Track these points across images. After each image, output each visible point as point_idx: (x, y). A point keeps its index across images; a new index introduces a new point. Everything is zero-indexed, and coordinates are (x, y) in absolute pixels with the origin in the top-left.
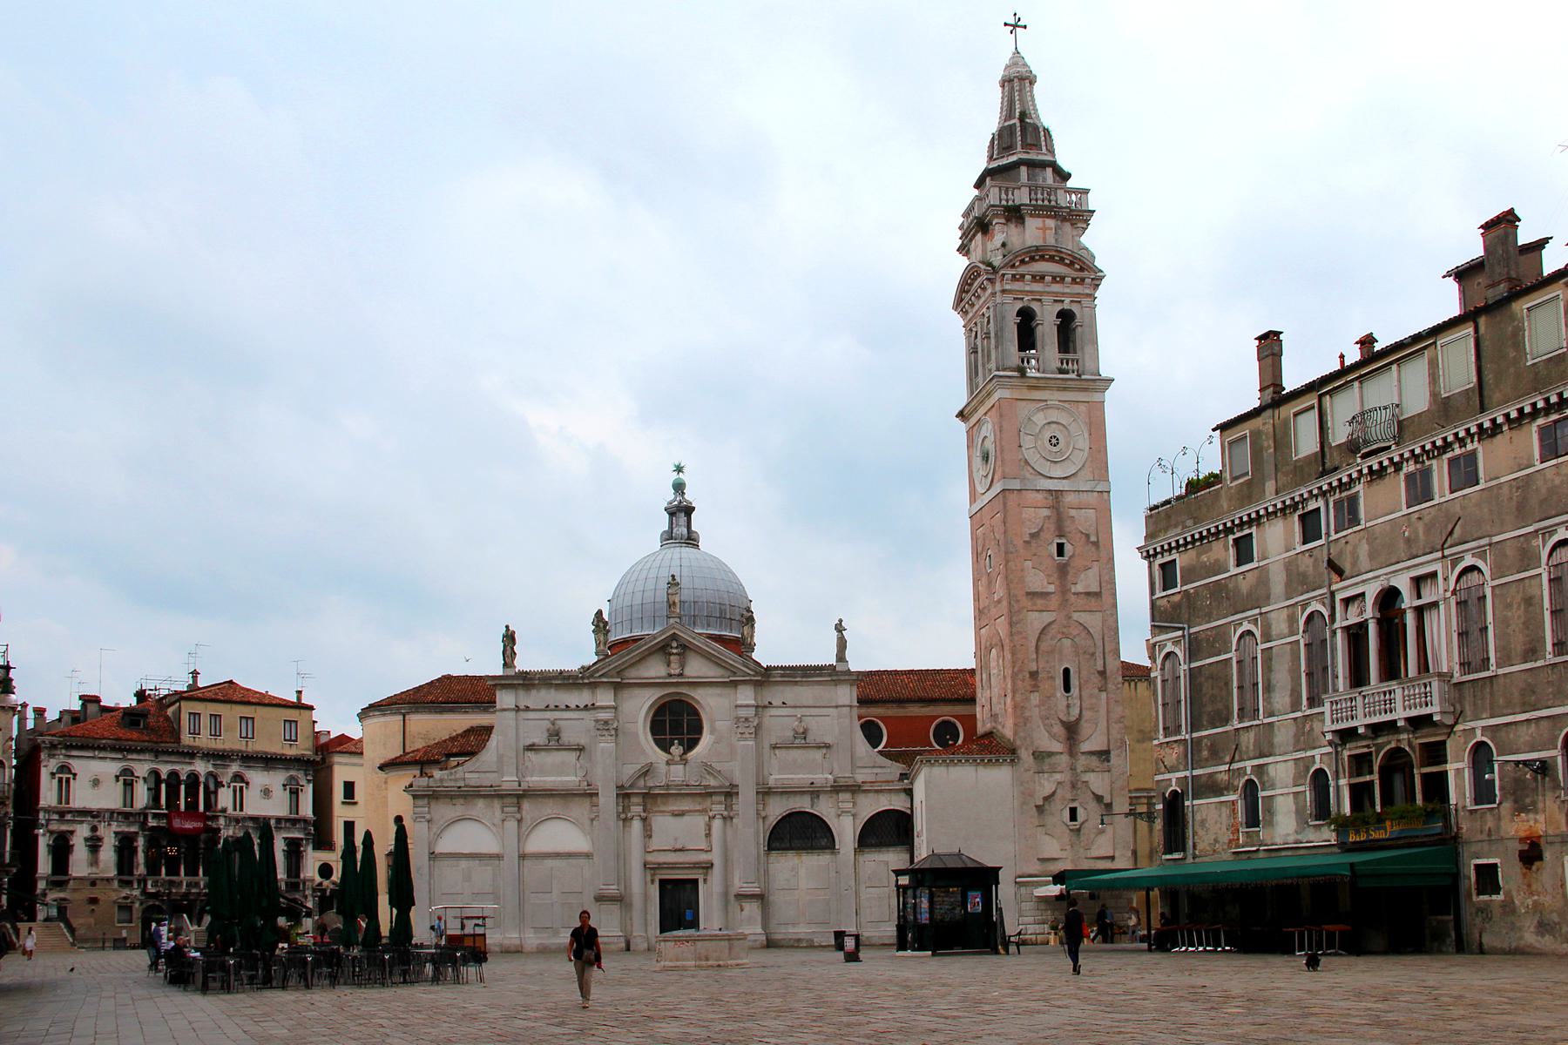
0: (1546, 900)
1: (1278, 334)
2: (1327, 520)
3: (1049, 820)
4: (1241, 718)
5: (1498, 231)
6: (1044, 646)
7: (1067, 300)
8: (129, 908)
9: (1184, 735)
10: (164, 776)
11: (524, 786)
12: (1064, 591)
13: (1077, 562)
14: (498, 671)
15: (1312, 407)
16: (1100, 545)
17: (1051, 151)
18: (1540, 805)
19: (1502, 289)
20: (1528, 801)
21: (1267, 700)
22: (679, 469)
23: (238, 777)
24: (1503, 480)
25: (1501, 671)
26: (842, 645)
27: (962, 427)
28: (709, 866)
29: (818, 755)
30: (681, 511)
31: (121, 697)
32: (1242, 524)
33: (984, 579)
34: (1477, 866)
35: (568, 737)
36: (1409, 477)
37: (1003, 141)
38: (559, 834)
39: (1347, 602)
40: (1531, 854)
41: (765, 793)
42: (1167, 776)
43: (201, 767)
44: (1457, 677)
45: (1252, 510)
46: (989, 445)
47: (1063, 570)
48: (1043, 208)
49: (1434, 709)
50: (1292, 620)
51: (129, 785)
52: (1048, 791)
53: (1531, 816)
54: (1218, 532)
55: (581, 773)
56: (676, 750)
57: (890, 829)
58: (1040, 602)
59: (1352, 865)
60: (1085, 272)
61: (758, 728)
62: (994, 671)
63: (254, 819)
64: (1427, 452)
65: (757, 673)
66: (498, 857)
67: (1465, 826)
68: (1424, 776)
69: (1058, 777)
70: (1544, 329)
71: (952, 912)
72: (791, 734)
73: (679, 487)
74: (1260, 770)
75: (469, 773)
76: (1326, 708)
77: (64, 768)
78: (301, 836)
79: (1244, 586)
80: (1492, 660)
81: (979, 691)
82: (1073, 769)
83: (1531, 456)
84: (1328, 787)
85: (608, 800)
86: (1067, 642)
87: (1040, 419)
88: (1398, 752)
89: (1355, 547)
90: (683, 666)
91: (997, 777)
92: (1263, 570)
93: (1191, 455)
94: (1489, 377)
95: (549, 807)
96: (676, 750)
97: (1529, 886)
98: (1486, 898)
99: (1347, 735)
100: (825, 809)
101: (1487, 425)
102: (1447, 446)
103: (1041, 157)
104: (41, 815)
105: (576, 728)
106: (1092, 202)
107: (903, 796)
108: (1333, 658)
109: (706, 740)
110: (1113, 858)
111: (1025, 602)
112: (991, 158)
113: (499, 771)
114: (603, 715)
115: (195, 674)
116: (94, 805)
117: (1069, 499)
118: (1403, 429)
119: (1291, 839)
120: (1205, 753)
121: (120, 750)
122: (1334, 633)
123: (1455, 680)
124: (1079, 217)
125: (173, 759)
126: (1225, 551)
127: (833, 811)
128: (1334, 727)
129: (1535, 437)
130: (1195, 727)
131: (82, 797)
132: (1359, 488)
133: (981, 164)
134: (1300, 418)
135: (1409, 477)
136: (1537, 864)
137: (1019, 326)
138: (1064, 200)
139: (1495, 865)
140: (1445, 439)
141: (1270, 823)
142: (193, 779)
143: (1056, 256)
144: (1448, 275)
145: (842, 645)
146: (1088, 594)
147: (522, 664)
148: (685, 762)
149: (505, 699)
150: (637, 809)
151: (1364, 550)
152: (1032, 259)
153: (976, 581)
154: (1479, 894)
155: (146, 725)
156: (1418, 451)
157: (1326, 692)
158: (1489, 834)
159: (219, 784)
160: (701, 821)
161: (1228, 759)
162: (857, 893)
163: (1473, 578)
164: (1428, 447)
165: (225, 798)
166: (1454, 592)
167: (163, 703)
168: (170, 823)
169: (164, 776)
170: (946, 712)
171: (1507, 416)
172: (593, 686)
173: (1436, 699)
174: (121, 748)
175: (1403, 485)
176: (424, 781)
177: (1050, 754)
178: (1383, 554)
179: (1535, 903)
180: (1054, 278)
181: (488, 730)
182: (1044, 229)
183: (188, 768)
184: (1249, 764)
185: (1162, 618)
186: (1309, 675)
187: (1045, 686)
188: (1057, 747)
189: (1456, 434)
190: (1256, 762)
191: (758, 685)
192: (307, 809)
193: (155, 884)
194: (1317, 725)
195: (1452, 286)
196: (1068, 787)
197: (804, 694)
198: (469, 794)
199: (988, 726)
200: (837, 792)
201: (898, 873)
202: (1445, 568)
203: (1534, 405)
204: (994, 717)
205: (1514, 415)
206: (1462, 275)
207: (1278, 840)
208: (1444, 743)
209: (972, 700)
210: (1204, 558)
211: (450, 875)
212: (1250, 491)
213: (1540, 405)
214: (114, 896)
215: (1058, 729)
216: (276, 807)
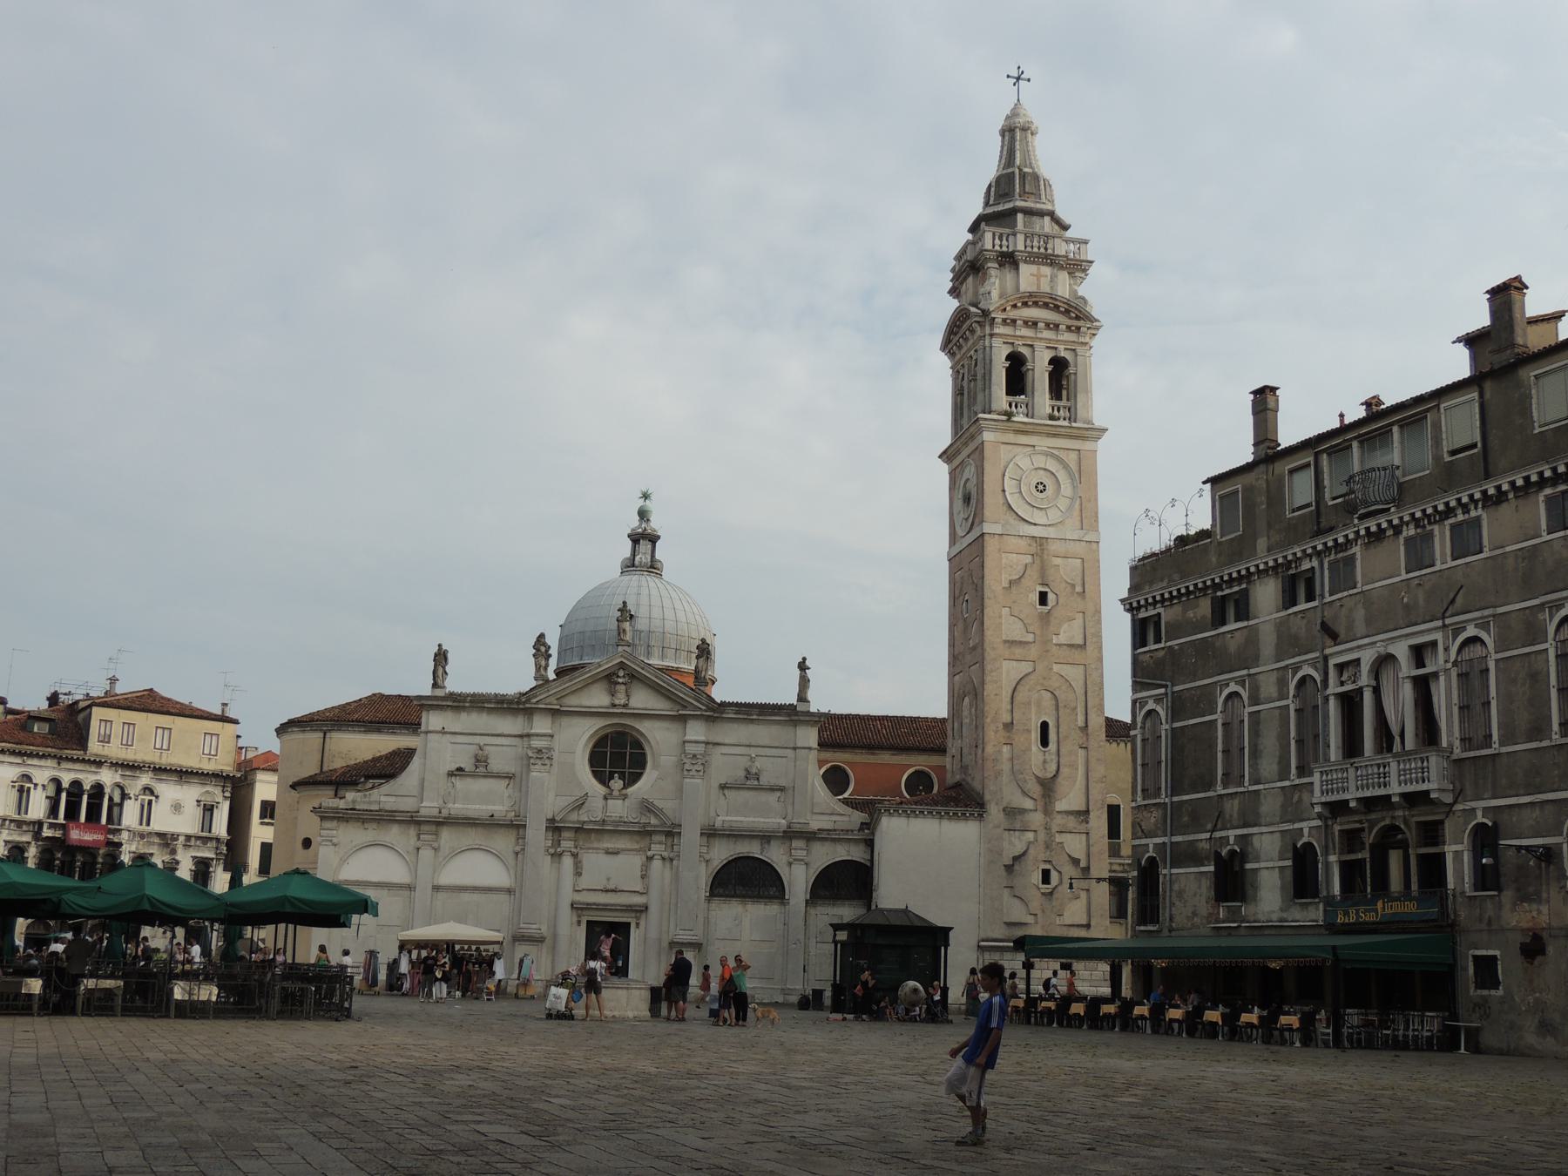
1: (1273, 389)
2: (1324, 580)
4: (1225, 785)
6: (1019, 697)
9: (1163, 798)
10: (65, 785)
11: (445, 813)
14: (426, 690)
15: (1307, 465)
18: (1544, 895)
20: (1531, 889)
22: (646, 496)
23: (148, 790)
24: (1508, 549)
25: (1504, 750)
26: (804, 682)
29: (772, 798)
30: (643, 538)
32: (1231, 580)
33: (960, 625)
34: (1475, 957)
35: (496, 765)
36: (1408, 540)
37: (1002, 187)
38: (479, 866)
39: (1341, 667)
40: (1533, 948)
42: (1144, 841)
43: (107, 777)
44: (1458, 752)
45: (1242, 568)
46: (972, 486)
47: (1045, 619)
48: (1038, 256)
50: (1282, 684)
51: (23, 793)
52: (1018, 850)
53: (1534, 906)
54: (1206, 588)
56: (617, 784)
57: (849, 881)
58: (1018, 651)
59: (1334, 948)
62: (966, 721)
63: (161, 835)
64: (1429, 516)
65: (709, 709)
67: (1463, 914)
68: (1421, 857)
70: (1553, 400)
71: (884, 964)
72: (742, 774)
73: (643, 514)
75: (383, 796)
78: (211, 855)
79: (1233, 645)
80: (1495, 737)
81: (950, 740)
82: (1047, 828)
84: (1317, 862)
85: (537, 834)
92: (1253, 630)
93: (1180, 509)
95: (472, 837)
96: (617, 784)
98: (1485, 992)
99: (1337, 809)
100: (776, 855)
101: (1491, 491)
102: (1449, 511)
103: (1039, 206)
105: (502, 757)
106: (1090, 253)
107: (862, 847)
108: (1326, 725)
110: (1088, 926)
112: (987, 204)
114: (536, 743)
117: (1053, 547)
118: (1402, 493)
119: (1275, 917)
122: (1326, 699)
123: (1454, 757)
125: (77, 766)
127: (785, 859)
128: (1360, 794)
129: (1542, 507)
130: (1175, 791)
133: (976, 208)
134: (1297, 477)
135: (1408, 540)
136: (1539, 959)
138: (1060, 248)
139: (1495, 957)
140: (1447, 504)
141: (1255, 899)
142: (98, 790)
143: (1051, 303)
144: (1459, 340)
145: (804, 682)
146: (1071, 646)
147: (456, 683)
148: (625, 797)
149: (433, 720)
150: (567, 844)
151: (1360, 614)
152: (1025, 304)
156: (1418, 515)
157: (1317, 761)
158: (1490, 923)
159: (124, 796)
160: (637, 861)
161: (1209, 826)
163: (1477, 650)
164: (1429, 511)
165: (130, 815)
166: (1455, 663)
169: (65, 785)
171: (1512, 483)
175: (1402, 548)
177: (1023, 811)
178: (1385, 616)
180: (1047, 325)
184: (1232, 834)
185: (1143, 675)
186: (1300, 742)
189: (1459, 500)
192: (220, 827)
194: (1305, 796)
195: (1463, 353)
198: (384, 818)
199: (958, 778)
200: (791, 839)
201: (837, 927)
202: (1446, 638)
203: (1541, 474)
205: (1520, 483)
206: (1472, 341)
207: (1260, 917)
208: (1442, 822)
209: (941, 750)
210: (1190, 614)
212: (1240, 548)
213: (1548, 474)
215: (1035, 789)
216: (186, 823)
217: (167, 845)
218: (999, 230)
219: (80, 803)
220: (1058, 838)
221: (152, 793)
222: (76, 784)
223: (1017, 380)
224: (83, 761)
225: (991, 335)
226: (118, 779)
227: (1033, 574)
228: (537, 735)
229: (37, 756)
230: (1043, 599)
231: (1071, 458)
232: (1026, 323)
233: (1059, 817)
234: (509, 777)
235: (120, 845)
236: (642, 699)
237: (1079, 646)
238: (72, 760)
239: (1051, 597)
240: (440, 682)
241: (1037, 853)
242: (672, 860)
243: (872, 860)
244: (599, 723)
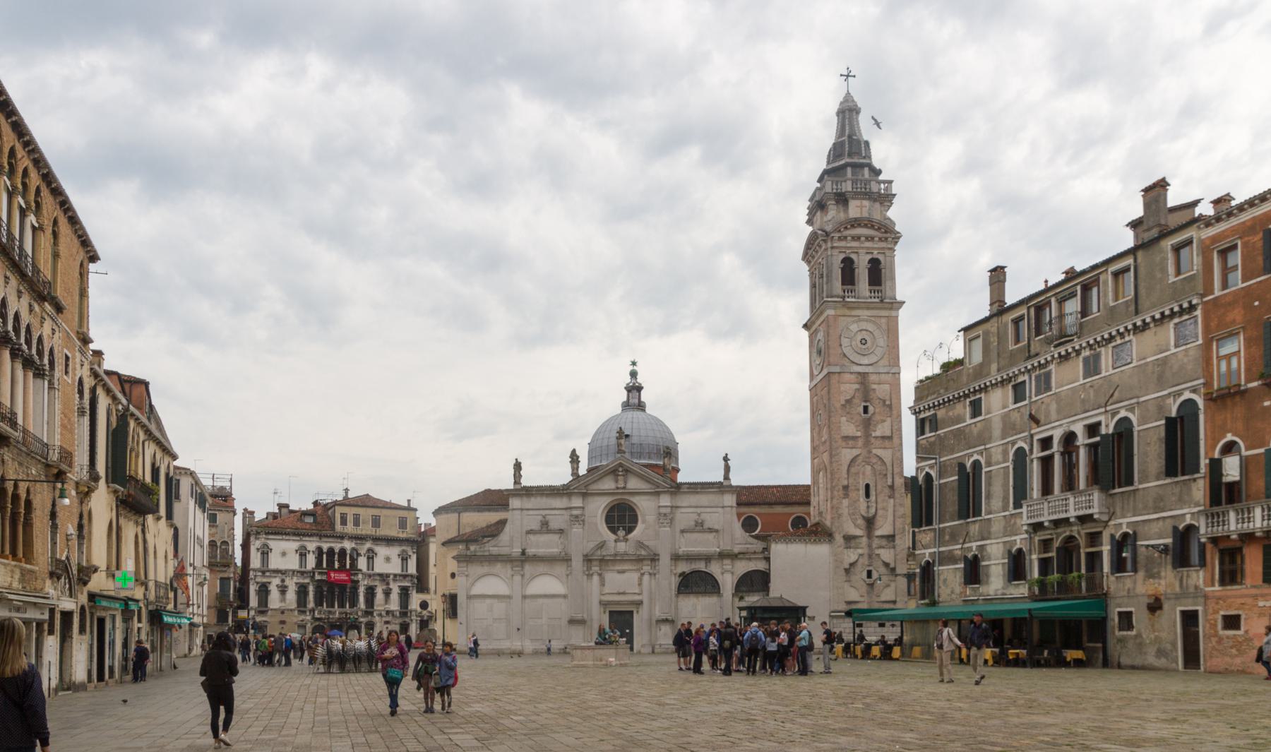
0: (1164, 635)
1: (1003, 268)
2: (1031, 388)
3: (854, 578)
5: (1153, 194)
6: (853, 470)
8: (304, 627)
12: (867, 435)
13: (877, 417)
14: (511, 486)
16: (891, 407)
17: (870, 158)
18: (1163, 574)
19: (1154, 233)
21: (988, 504)
22: (634, 364)
27: (805, 334)
28: (640, 603)
30: (634, 389)
31: (302, 503)
34: (1120, 613)
35: (554, 524)
37: (836, 151)
38: (547, 583)
41: (676, 558)
43: (348, 545)
48: (860, 193)
49: (1095, 510)
50: (1005, 453)
56: (621, 533)
57: (757, 581)
60: (888, 234)
61: (672, 520)
66: (509, 597)
67: (1112, 588)
68: (1088, 554)
69: (860, 551)
73: (634, 374)
74: (981, 548)
76: (1024, 509)
82: (870, 546)
83: (1168, 344)
85: (577, 563)
86: (869, 468)
87: (854, 327)
88: (1071, 538)
89: (1048, 405)
90: (626, 482)
91: (819, 552)
94: (1142, 291)
95: (542, 568)
96: (621, 533)
97: (1153, 626)
98: (1125, 633)
99: (1037, 527)
100: (715, 569)
101: (1139, 323)
102: (1112, 338)
105: (557, 521)
109: (640, 527)
110: (894, 602)
111: (840, 442)
112: (828, 163)
113: (511, 546)
114: (575, 512)
115: (347, 490)
116: (282, 567)
117: (873, 378)
120: (947, 537)
121: (298, 535)
124: (886, 199)
126: (964, 409)
129: (1172, 331)
131: (275, 562)
132: (1052, 367)
133: (822, 165)
137: (870, 270)
139: (1131, 613)
141: (987, 583)
142: (343, 552)
143: (868, 223)
146: (883, 438)
147: (525, 482)
148: (627, 540)
149: (515, 503)
150: (595, 569)
151: (1054, 407)
152: (853, 226)
153: (812, 430)
154: (1120, 629)
155: (319, 520)
159: (359, 555)
160: (636, 576)
165: (362, 563)
167: (327, 507)
168: (329, 576)
170: (798, 511)
171: (1153, 317)
173: (1096, 503)
174: (298, 534)
177: (855, 537)
179: (1156, 637)
181: (503, 523)
182: (861, 207)
183: (328, 545)
184: (974, 545)
187: (853, 494)
188: (859, 532)
190: (979, 543)
191: (672, 493)
192: (412, 569)
193: (320, 613)
196: (866, 557)
197: (703, 499)
199: (817, 519)
202: (1107, 419)
203: (1172, 309)
204: (820, 514)
206: (1135, 225)
208: (1100, 533)
209: (808, 503)
211: (480, 608)
214: (295, 620)
215: (860, 522)
216: (394, 567)
222: (331, 551)
234: (561, 531)
236: (634, 483)
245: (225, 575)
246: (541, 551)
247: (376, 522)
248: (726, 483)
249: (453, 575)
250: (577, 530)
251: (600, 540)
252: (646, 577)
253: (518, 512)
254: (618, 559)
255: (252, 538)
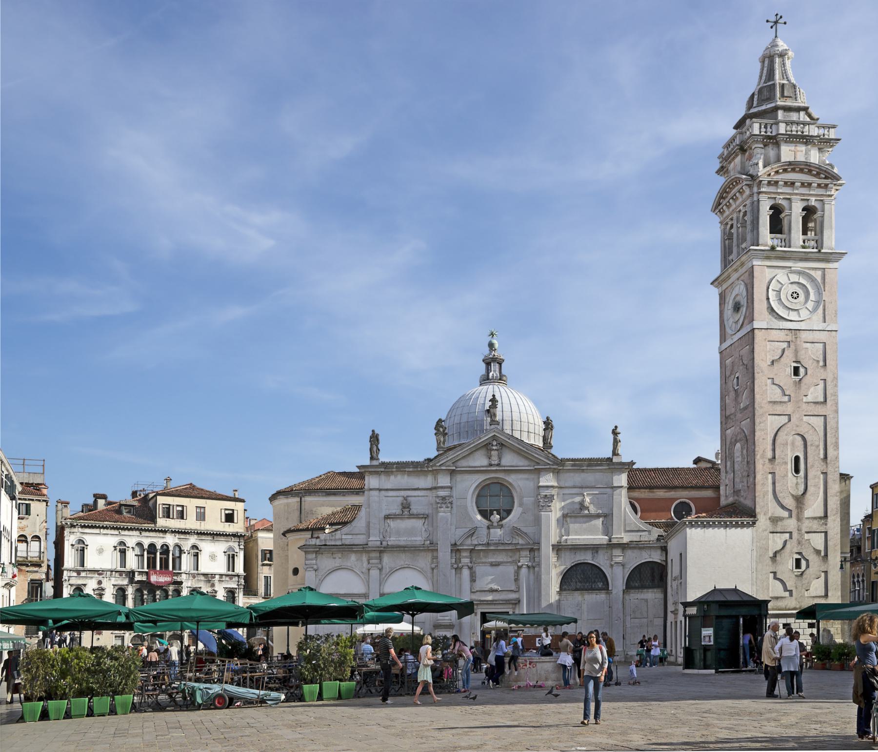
7: (741, 208)
10: (146, 547)
23: (194, 547)
26: (616, 442)
35: (415, 509)
48: (796, 136)
55: (425, 535)
57: (653, 576)
63: (204, 575)
75: (344, 536)
77: (80, 541)
82: (799, 530)
85: (445, 554)
90: (500, 459)
95: (404, 559)
100: (601, 561)
104: (65, 573)
107: (659, 552)
109: (516, 512)
114: (442, 493)
125: (152, 534)
142: (165, 550)
143: (806, 168)
146: (816, 403)
147: (384, 457)
148: (501, 526)
152: (785, 171)
160: (511, 569)
162: (624, 622)
165: (186, 562)
169: (146, 547)
172: (436, 473)
176: (313, 542)
177: (781, 519)
191: (557, 472)
192: (240, 568)
198: (346, 549)
199: (731, 500)
204: (736, 492)
215: (790, 503)
217: (209, 581)
218: (765, 121)
219: (159, 558)
220: (806, 536)
221: (197, 548)
222: (152, 546)
223: (777, 225)
224: (155, 531)
225: (759, 193)
226: (177, 541)
227: (789, 355)
228: (442, 487)
229: (127, 529)
230: (796, 371)
231: (818, 275)
232: (786, 183)
233: (807, 521)
234: (425, 517)
235: (181, 583)
237: (822, 403)
238: (148, 530)
239: (802, 371)
240: (375, 455)
241: (792, 547)
242: (534, 567)
243: (666, 561)
244: (479, 478)
245: (36, 576)
246: (403, 541)
247: (201, 516)
248: (615, 460)
249: (296, 571)
250: (443, 514)
251: (470, 526)
252: (524, 571)
253: (376, 493)
254: (490, 547)
255: (67, 532)
